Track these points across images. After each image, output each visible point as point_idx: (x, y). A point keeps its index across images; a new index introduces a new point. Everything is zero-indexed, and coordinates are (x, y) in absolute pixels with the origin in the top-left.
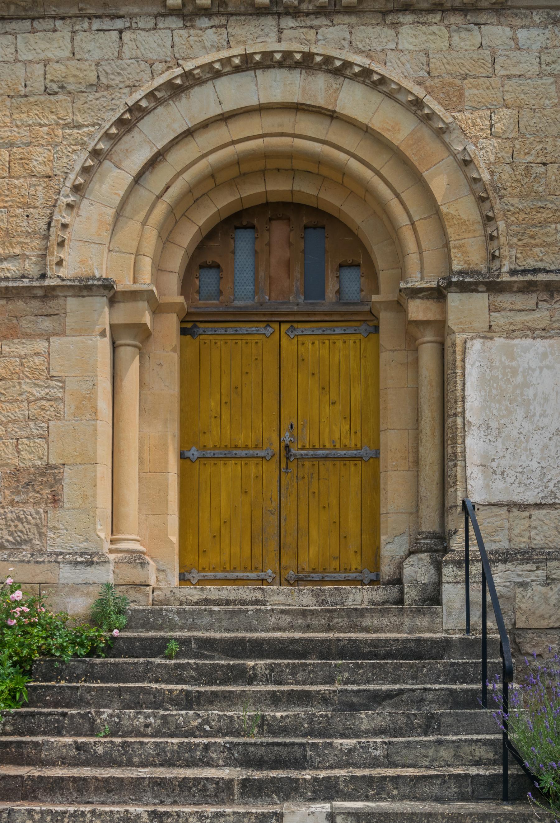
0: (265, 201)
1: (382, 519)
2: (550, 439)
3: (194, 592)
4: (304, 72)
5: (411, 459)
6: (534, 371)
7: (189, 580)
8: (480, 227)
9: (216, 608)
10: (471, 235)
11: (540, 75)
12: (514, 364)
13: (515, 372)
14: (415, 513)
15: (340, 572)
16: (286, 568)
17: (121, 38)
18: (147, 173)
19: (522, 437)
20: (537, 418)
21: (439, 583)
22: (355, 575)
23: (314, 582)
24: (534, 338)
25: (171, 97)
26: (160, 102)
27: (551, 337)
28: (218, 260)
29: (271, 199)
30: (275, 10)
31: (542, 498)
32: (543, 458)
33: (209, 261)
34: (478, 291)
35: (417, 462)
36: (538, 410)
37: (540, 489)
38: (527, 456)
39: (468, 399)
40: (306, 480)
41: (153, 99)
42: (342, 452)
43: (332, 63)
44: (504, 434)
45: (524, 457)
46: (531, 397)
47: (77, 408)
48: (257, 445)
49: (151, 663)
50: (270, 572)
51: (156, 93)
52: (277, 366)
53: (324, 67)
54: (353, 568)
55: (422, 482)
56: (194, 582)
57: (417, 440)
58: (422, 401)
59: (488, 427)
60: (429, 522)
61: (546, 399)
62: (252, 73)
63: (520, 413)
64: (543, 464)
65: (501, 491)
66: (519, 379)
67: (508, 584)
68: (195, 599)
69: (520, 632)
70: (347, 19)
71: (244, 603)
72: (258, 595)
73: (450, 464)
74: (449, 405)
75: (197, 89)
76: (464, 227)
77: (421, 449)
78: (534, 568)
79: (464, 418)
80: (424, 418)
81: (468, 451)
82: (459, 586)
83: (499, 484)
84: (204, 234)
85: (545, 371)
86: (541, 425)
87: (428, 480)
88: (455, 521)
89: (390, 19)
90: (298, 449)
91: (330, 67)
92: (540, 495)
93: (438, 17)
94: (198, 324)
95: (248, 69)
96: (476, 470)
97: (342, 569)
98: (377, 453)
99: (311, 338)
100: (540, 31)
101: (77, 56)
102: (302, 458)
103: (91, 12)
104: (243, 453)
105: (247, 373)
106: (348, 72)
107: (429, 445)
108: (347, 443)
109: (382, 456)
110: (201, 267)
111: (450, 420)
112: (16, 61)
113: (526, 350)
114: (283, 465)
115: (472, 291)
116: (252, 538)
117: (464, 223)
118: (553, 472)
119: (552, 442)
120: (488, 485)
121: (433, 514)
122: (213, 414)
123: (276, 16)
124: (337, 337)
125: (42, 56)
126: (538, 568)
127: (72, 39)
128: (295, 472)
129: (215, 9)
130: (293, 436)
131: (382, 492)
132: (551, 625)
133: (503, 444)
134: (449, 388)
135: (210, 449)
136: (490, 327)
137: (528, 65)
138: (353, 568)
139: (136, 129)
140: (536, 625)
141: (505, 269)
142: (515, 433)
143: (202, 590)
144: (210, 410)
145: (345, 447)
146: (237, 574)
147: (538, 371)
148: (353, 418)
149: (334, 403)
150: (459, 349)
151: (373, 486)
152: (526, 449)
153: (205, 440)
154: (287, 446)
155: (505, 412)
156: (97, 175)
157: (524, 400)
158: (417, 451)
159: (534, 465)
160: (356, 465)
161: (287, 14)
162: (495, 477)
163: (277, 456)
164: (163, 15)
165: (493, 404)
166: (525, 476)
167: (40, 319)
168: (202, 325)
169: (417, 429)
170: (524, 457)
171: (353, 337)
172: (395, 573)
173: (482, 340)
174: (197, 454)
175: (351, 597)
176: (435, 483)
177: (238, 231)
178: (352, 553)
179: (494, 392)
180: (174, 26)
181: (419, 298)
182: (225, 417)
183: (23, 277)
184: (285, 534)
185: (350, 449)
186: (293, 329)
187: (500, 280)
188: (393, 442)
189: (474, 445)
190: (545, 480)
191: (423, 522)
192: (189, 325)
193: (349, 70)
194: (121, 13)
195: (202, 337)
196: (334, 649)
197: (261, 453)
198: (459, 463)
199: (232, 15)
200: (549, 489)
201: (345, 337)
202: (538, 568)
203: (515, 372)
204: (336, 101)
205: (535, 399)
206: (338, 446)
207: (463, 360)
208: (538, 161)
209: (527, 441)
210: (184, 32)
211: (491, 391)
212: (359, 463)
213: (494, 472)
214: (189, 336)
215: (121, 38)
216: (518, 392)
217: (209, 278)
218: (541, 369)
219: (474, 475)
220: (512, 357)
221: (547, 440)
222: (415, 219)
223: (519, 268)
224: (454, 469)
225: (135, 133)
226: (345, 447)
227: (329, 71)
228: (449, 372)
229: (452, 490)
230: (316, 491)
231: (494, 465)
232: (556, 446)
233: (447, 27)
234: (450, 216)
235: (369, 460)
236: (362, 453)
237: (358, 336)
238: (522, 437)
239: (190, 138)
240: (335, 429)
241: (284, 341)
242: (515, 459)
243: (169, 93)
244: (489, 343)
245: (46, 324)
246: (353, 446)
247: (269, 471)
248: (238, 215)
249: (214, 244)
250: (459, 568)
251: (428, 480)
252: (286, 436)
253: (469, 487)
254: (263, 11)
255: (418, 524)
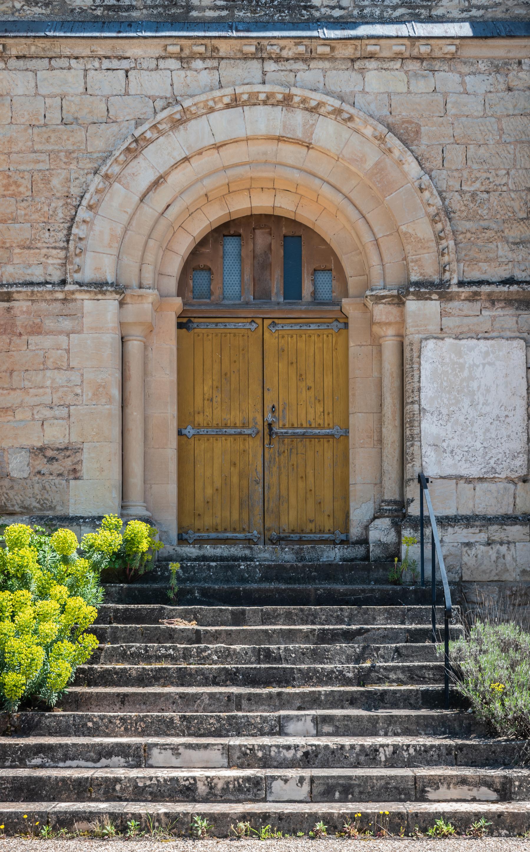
0: (249, 214)
1: (351, 488)
2: (491, 423)
3: (193, 550)
4: (284, 109)
5: (376, 438)
6: (478, 366)
7: (186, 540)
8: (434, 244)
9: (213, 564)
10: (425, 251)
11: (484, 116)
12: (461, 361)
13: (462, 367)
14: (379, 484)
15: (315, 533)
16: (269, 530)
17: (127, 76)
18: (150, 193)
19: (468, 422)
20: (480, 406)
21: (399, 543)
22: (327, 536)
23: (293, 542)
24: (478, 339)
25: (171, 128)
26: (161, 133)
27: (492, 338)
28: (209, 264)
29: (255, 212)
30: (259, 55)
31: (485, 473)
32: (485, 440)
33: (202, 265)
34: (432, 300)
35: (380, 441)
36: (481, 400)
37: (483, 465)
38: (472, 438)
39: (423, 390)
40: (286, 454)
41: (156, 131)
42: (317, 431)
43: (309, 103)
44: (452, 420)
45: (469, 439)
46: (475, 388)
47: (94, 394)
48: (244, 424)
49: (165, 608)
50: (255, 532)
51: (158, 126)
52: (260, 356)
53: (302, 105)
54: (327, 530)
55: (384, 458)
56: (190, 542)
57: (381, 422)
58: (385, 389)
59: (440, 413)
60: (391, 492)
61: (488, 390)
62: (240, 109)
63: (466, 402)
64: (485, 444)
65: (449, 466)
66: (466, 373)
67: (456, 544)
68: (194, 556)
69: (467, 585)
70: (321, 64)
71: (235, 559)
72: (247, 552)
73: (408, 443)
74: (407, 394)
75: (193, 122)
76: (420, 245)
77: (384, 430)
78: (477, 531)
79: (420, 405)
80: (386, 404)
81: (422, 433)
82: (416, 546)
83: (448, 461)
84: (197, 241)
85: (487, 366)
86: (483, 411)
87: (390, 456)
88: (412, 491)
89: (357, 65)
90: (279, 428)
91: (307, 106)
92: (483, 471)
93: (398, 65)
94: (192, 319)
95: (237, 106)
96: (429, 448)
97: (318, 531)
98: (347, 432)
99: (290, 332)
100: (485, 77)
101: (89, 91)
102: (283, 436)
103: (102, 53)
104: (232, 431)
105: (235, 362)
106: (322, 110)
107: (390, 427)
108: (321, 422)
109: (351, 435)
110: (194, 269)
111: (408, 407)
112: (36, 94)
113: (471, 349)
114: (267, 442)
115: (426, 299)
116: (241, 504)
117: (420, 241)
118: (494, 451)
119: (493, 426)
120: (440, 462)
121: (394, 485)
122: (206, 397)
123: (260, 61)
124: (312, 332)
125: (59, 91)
126: (480, 531)
127: (85, 76)
128: (277, 446)
129: (209, 54)
130: (275, 417)
131: (351, 466)
132: (491, 579)
133: (452, 427)
134: (407, 380)
135: (203, 427)
136: (442, 329)
137: (474, 106)
138: (327, 530)
139: (141, 156)
140: (479, 579)
141: (455, 281)
142: (462, 419)
143: (200, 548)
144: (204, 394)
145: (319, 426)
146: (228, 534)
147: (481, 368)
148: (326, 402)
149: (309, 388)
150: (415, 348)
151: (344, 460)
152: (471, 432)
153: (199, 419)
154: (270, 425)
155: (454, 401)
156: (108, 195)
157: (469, 391)
158: (381, 432)
159: (478, 445)
160: (329, 441)
161: (270, 58)
162: (445, 455)
163: (261, 434)
164: (163, 58)
165: (444, 395)
166: (470, 454)
167: (60, 319)
168: (196, 320)
169: (381, 413)
170: (469, 439)
171: (326, 332)
172: (362, 534)
173: (435, 341)
174: (192, 432)
175: (325, 554)
176: (396, 458)
177: (226, 238)
178: (326, 517)
179: (445, 384)
180: (172, 68)
181: (382, 303)
182: (217, 399)
183: (47, 283)
184: (268, 501)
185: (323, 428)
186: (274, 324)
187: (449, 290)
188: (360, 422)
189: (429, 427)
190: (487, 458)
191: (386, 491)
192: (185, 320)
193: (323, 108)
194: (127, 55)
195: (196, 330)
196: (312, 598)
197: (247, 431)
198: (416, 443)
199: (222, 58)
200: (490, 465)
201: (318, 332)
202: (480, 531)
203: (462, 367)
204: (312, 134)
205: (478, 390)
206: (313, 426)
207: (419, 357)
208: (483, 188)
209: (472, 425)
210: (182, 73)
211: (442, 383)
212: (331, 440)
213: (445, 451)
214: (184, 330)
215: (127, 76)
216: (465, 384)
217: (201, 278)
218: (484, 365)
219: (428, 453)
220: (459, 354)
221: (488, 425)
222: (379, 235)
223: (465, 280)
224: (412, 448)
225: (140, 159)
226: (319, 426)
227: (306, 109)
228: (408, 366)
229: (410, 465)
230: (295, 463)
231: (445, 445)
232: (496, 430)
233: (406, 72)
234: (408, 235)
235: (340, 437)
236: (334, 431)
237: (330, 331)
238: (468, 422)
239: (187, 163)
240: (311, 411)
241: (266, 335)
242: (462, 440)
243: (169, 125)
244: (440, 343)
245: (67, 324)
246: (326, 425)
247: (254, 446)
248: (226, 225)
249: (206, 250)
250: (416, 531)
251: (390, 456)
252: (269, 417)
253: (424, 463)
254: (250, 56)
255: (382, 493)
